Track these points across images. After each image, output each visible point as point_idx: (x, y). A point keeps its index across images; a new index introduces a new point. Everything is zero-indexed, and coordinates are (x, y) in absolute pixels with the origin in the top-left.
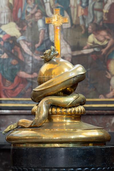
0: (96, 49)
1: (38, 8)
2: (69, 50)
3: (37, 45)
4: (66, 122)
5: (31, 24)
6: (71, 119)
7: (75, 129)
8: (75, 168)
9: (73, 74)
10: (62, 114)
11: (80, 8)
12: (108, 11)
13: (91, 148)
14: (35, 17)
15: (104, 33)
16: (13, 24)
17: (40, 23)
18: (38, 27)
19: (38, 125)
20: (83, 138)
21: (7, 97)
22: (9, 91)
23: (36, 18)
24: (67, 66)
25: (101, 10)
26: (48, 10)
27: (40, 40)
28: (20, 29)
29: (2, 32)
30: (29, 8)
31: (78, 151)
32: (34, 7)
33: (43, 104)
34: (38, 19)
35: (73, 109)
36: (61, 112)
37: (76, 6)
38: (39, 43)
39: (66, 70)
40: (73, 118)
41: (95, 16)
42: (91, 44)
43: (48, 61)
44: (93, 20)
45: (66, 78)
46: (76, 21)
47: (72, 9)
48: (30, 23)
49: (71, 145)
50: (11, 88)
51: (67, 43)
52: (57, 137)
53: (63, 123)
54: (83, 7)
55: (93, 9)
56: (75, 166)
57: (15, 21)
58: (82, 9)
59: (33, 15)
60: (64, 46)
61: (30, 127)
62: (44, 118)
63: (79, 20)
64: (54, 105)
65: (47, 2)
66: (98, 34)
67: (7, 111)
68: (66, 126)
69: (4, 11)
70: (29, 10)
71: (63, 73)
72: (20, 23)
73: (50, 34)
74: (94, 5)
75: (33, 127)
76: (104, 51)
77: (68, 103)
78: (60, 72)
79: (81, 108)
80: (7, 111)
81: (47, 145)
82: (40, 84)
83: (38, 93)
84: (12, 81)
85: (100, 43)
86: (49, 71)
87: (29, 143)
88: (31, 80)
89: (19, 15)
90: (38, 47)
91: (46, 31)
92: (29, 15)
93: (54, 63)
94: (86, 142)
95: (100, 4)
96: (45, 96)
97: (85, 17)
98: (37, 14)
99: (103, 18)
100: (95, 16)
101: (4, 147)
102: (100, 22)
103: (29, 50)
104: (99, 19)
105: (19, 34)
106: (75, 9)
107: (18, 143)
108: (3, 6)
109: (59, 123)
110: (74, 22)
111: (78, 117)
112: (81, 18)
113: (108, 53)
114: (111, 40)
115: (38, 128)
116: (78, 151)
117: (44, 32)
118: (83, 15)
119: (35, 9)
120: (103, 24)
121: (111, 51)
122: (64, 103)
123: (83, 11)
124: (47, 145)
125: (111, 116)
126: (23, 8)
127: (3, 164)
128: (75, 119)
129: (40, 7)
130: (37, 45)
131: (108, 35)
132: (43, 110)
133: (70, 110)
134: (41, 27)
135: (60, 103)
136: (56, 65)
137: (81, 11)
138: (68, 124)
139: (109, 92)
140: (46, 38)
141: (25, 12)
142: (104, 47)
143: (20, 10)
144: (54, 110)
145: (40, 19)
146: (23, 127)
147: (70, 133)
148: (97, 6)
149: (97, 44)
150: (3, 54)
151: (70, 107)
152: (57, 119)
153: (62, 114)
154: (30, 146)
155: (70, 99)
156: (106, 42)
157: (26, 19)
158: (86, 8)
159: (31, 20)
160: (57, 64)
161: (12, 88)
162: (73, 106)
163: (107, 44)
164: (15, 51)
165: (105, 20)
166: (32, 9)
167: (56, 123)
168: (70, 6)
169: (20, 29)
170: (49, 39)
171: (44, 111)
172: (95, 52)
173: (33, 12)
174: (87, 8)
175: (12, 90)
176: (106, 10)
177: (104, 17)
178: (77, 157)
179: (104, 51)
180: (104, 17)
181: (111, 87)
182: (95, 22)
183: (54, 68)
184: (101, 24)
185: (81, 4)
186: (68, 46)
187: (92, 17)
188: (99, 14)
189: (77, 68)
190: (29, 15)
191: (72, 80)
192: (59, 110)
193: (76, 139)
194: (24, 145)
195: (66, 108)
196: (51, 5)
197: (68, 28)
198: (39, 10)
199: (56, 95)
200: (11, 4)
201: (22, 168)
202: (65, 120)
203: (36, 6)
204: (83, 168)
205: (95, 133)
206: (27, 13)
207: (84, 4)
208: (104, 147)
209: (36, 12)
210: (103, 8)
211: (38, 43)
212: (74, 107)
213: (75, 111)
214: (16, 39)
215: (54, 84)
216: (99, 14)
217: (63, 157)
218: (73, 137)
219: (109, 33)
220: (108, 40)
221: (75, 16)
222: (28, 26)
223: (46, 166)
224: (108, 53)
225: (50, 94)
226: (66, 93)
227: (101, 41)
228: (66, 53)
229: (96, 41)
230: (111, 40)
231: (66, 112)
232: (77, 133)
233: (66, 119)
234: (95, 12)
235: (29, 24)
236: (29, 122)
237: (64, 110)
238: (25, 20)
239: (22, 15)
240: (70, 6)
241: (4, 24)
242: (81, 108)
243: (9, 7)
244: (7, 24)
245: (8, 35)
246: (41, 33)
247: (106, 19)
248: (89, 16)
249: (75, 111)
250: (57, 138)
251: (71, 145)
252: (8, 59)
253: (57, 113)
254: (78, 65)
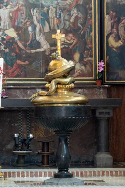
0: (66, 46)
1: (28, 19)
2: (49, 46)
3: (28, 43)
4: (64, 93)
5: (24, 30)
6: (67, 91)
7: (70, 96)
8: (71, 117)
9: (68, 67)
10: (63, 88)
11: (56, 19)
12: (73, 21)
13: (79, 107)
14: (26, 25)
15: (71, 35)
16: (12, 30)
17: (30, 29)
18: (28, 31)
19: (51, 94)
20: (75, 101)
21: (9, 77)
22: (10, 73)
23: (27, 25)
24: (64, 62)
25: (69, 20)
26: (35, 20)
27: (30, 40)
28: (17, 33)
29: (6, 34)
30: (22, 19)
31: (73, 108)
32: (26, 18)
33: (53, 83)
34: (29, 26)
35: (69, 85)
36: (62, 87)
37: (53, 17)
38: (30, 42)
39: (64, 64)
40: (68, 90)
41: (65, 24)
42: (63, 43)
43: (54, 59)
44: (64, 27)
45: (65, 69)
46: (53, 27)
47: (50, 20)
48: (24, 28)
49: (68, 105)
50: (11, 71)
51: (48, 42)
52: (60, 101)
53: (63, 93)
54: (58, 18)
55: (64, 20)
56: (71, 116)
57: (13, 28)
58: (56, 20)
59: (25, 23)
60: (46, 43)
61: (46, 95)
62: (54, 90)
63: (55, 27)
64: (59, 83)
65: (34, 15)
66: (67, 36)
67: (12, 86)
68: (65, 94)
69: (6, 21)
70: (22, 20)
71: (63, 66)
72: (17, 29)
73: (37, 36)
74: (64, 17)
75: (48, 95)
76: (71, 47)
77: (66, 82)
78: (61, 65)
79: (72, 85)
80: (12, 86)
81: (55, 105)
82: (50, 72)
83: (49, 77)
84: (12, 67)
85: (68, 42)
86: (55, 65)
87: (47, 104)
88: (24, 66)
89: (16, 24)
90: (29, 44)
91: (34, 34)
92: (23, 23)
93: (58, 60)
94: (76, 103)
95: (68, 16)
96: (54, 78)
97: (58, 25)
98: (28, 23)
99: (70, 26)
100: (65, 24)
101: (12, 109)
102: (68, 28)
103: (22, 46)
104: (67, 26)
105: (16, 36)
106: (53, 20)
107: (40, 104)
108: (6, 18)
109: (61, 93)
110: (52, 28)
111: (71, 89)
112: (56, 25)
113: (74, 48)
114: (76, 40)
115: (51, 96)
116: (73, 108)
117: (33, 35)
118: (57, 24)
119: (26, 20)
120: (70, 29)
121: (76, 46)
122: (64, 82)
123: (57, 21)
124: (55, 105)
125: (77, 89)
126: (19, 19)
127: (8, 120)
128: (70, 91)
129: (30, 18)
130: (28, 43)
131: (73, 37)
132: (53, 86)
133: (67, 86)
134: (31, 32)
135: (62, 82)
136: (59, 61)
137: (56, 21)
138: (65, 93)
139: (74, 73)
140: (34, 39)
141: (20, 22)
142: (71, 44)
143: (17, 20)
144: (59, 86)
145: (30, 26)
146: (42, 96)
147: (67, 98)
148: (67, 18)
149: (67, 42)
150: (6, 49)
151: (67, 84)
152: (60, 91)
153: (63, 88)
154: (45, 105)
155: (68, 80)
156: (72, 41)
157: (21, 27)
158: (59, 19)
159: (24, 27)
160: (59, 60)
161: (12, 71)
162: (69, 83)
163: (73, 42)
164: (14, 47)
165: (71, 27)
166: (24, 19)
167: (59, 93)
168: (49, 18)
169: (17, 33)
170: (36, 39)
171: (54, 87)
172: (65, 47)
173: (25, 22)
174: (60, 19)
175: (12, 72)
176: (72, 20)
177: (71, 25)
178: (73, 111)
179: (71, 47)
180: (71, 25)
181: (76, 70)
182: (65, 28)
183: (57, 63)
184: (69, 29)
185: (56, 17)
186: (48, 44)
187: (63, 25)
188: (67, 23)
189: (70, 63)
190: (23, 23)
191: (68, 70)
192: (61, 86)
193: (71, 101)
194: (42, 105)
195: (65, 85)
196: (37, 17)
197: (47, 32)
198: (29, 21)
199: (59, 78)
200: (11, 16)
201: (42, 118)
202: (64, 92)
203: (27, 18)
204: (76, 117)
205: (80, 98)
206: (22, 22)
207: (58, 17)
208: (86, 106)
209: (27, 22)
210: (70, 19)
211: (28, 42)
212: (69, 84)
213: (70, 86)
214: (15, 39)
215: (59, 72)
216: (67, 23)
217: (103, 98)
218: (69, 100)
219: (74, 35)
220: (74, 40)
221: (52, 24)
222: (22, 31)
223: (56, 116)
224: (74, 48)
225: (56, 77)
226: (65, 77)
227: (69, 40)
228: (47, 48)
229: (66, 41)
230: (76, 40)
231: (65, 87)
232: (71, 98)
233: (65, 91)
234: (65, 22)
235: (23, 30)
236: (46, 93)
237: (64, 86)
238: (20, 27)
239: (18, 24)
240: (49, 18)
241: (7, 30)
242: (72, 85)
243: (10, 18)
244: (8, 29)
245: (10, 37)
246: (30, 35)
247: (72, 26)
248: (61, 24)
249: (70, 86)
250: (61, 101)
251: (68, 105)
252: (9, 52)
253: (61, 88)
254: (70, 61)
